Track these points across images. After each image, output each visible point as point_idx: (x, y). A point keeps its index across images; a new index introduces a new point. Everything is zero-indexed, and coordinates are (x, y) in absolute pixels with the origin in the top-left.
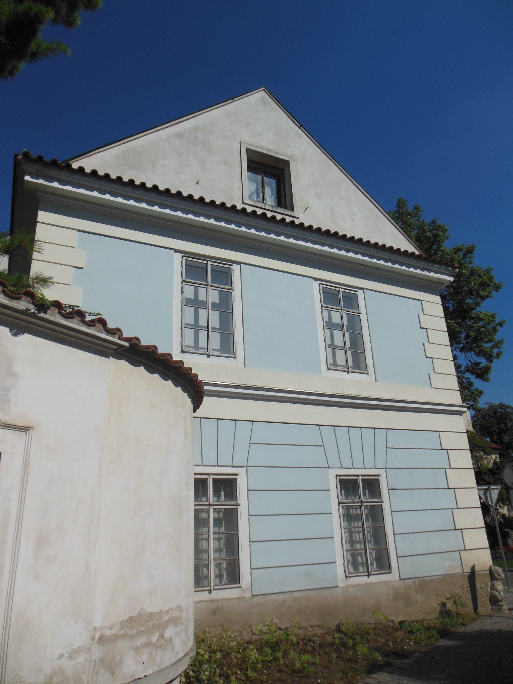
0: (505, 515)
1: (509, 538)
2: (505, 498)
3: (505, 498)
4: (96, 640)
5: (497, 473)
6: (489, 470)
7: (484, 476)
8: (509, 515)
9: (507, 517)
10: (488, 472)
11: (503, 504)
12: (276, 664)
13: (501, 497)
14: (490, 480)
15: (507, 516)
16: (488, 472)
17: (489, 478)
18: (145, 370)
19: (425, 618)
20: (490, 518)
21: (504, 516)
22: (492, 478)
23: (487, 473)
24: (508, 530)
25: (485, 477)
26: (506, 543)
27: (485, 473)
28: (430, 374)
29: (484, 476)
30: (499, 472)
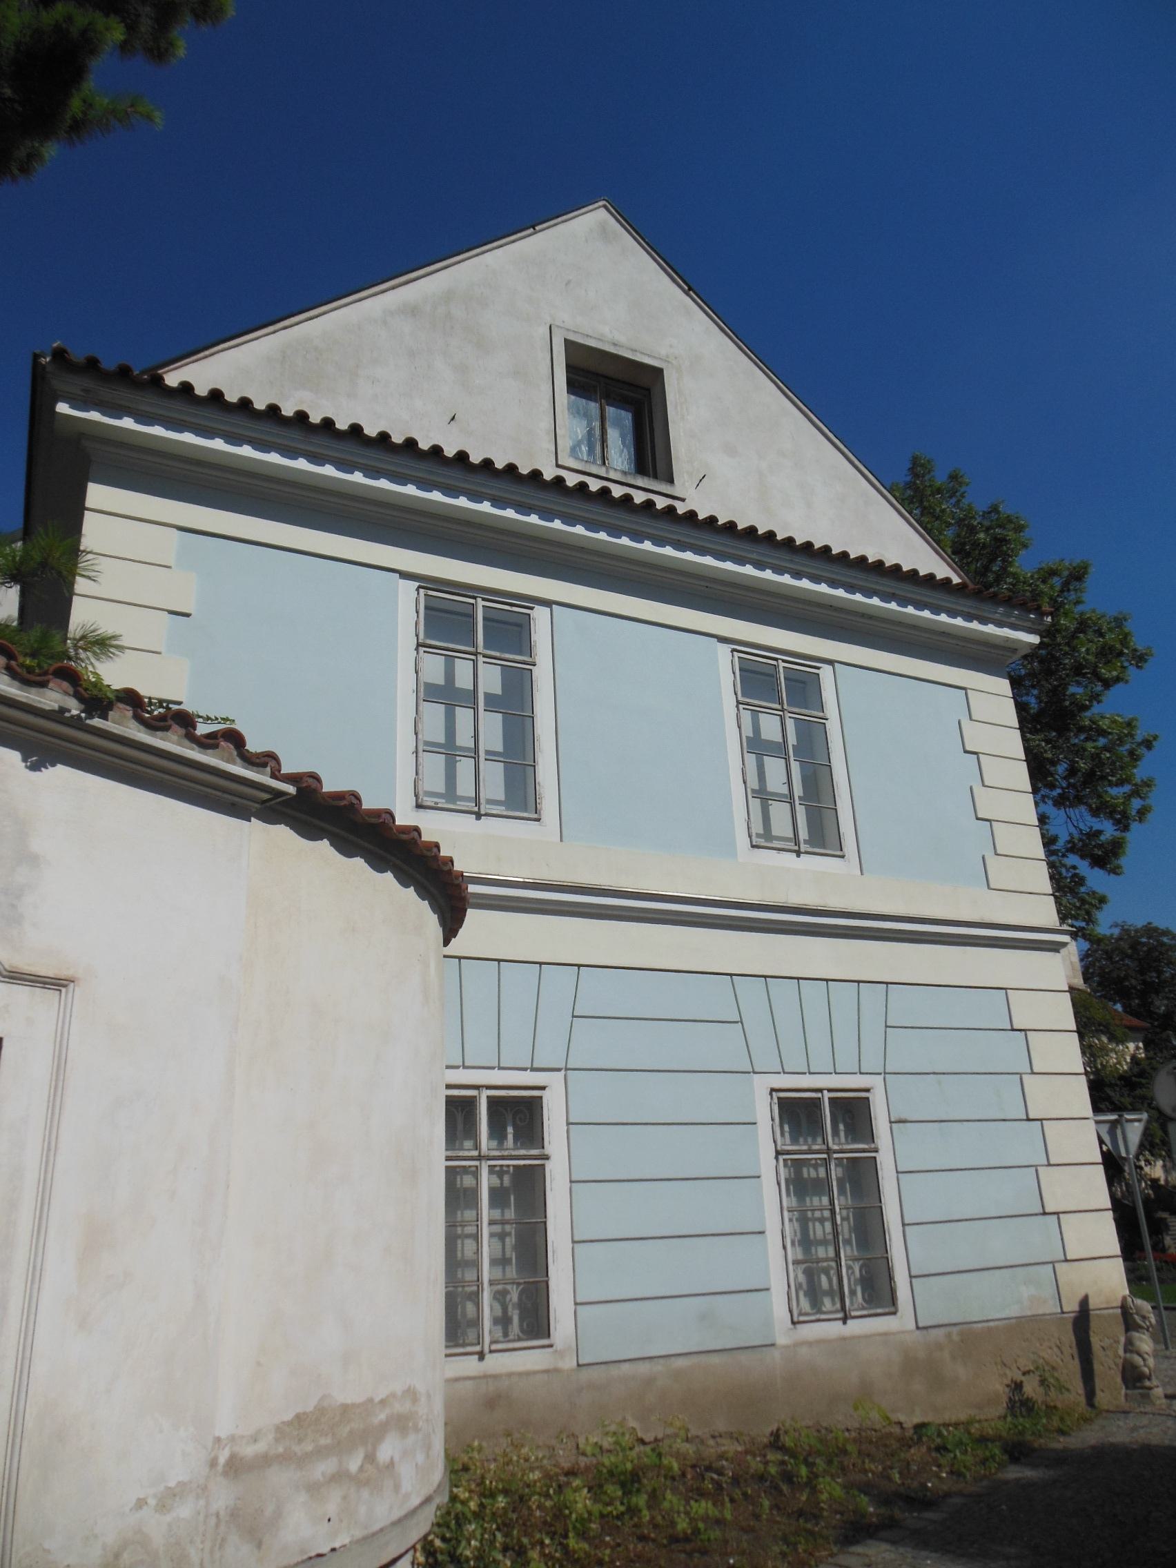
0: (1157, 1180)
1: (1168, 1234)
2: (1157, 1141)
3: (1157, 1141)
4: (220, 1468)
5: (1140, 1083)
6: (1122, 1077)
7: (1109, 1091)
8: (1166, 1180)
9: (1162, 1186)
10: (1118, 1082)
11: (1152, 1155)
12: (632, 1523)
13: (1150, 1138)
14: (1123, 1100)
15: (1162, 1182)
16: (1118, 1082)
17: (1122, 1096)
18: (332, 848)
19: (975, 1416)
20: (1124, 1188)
21: (1154, 1182)
22: (1129, 1095)
23: (1117, 1085)
24: (1165, 1215)
25: (1111, 1094)
26: (1161, 1245)
27: (1111, 1085)
28: (986, 857)
29: (1109, 1091)
30: (1143, 1081)
